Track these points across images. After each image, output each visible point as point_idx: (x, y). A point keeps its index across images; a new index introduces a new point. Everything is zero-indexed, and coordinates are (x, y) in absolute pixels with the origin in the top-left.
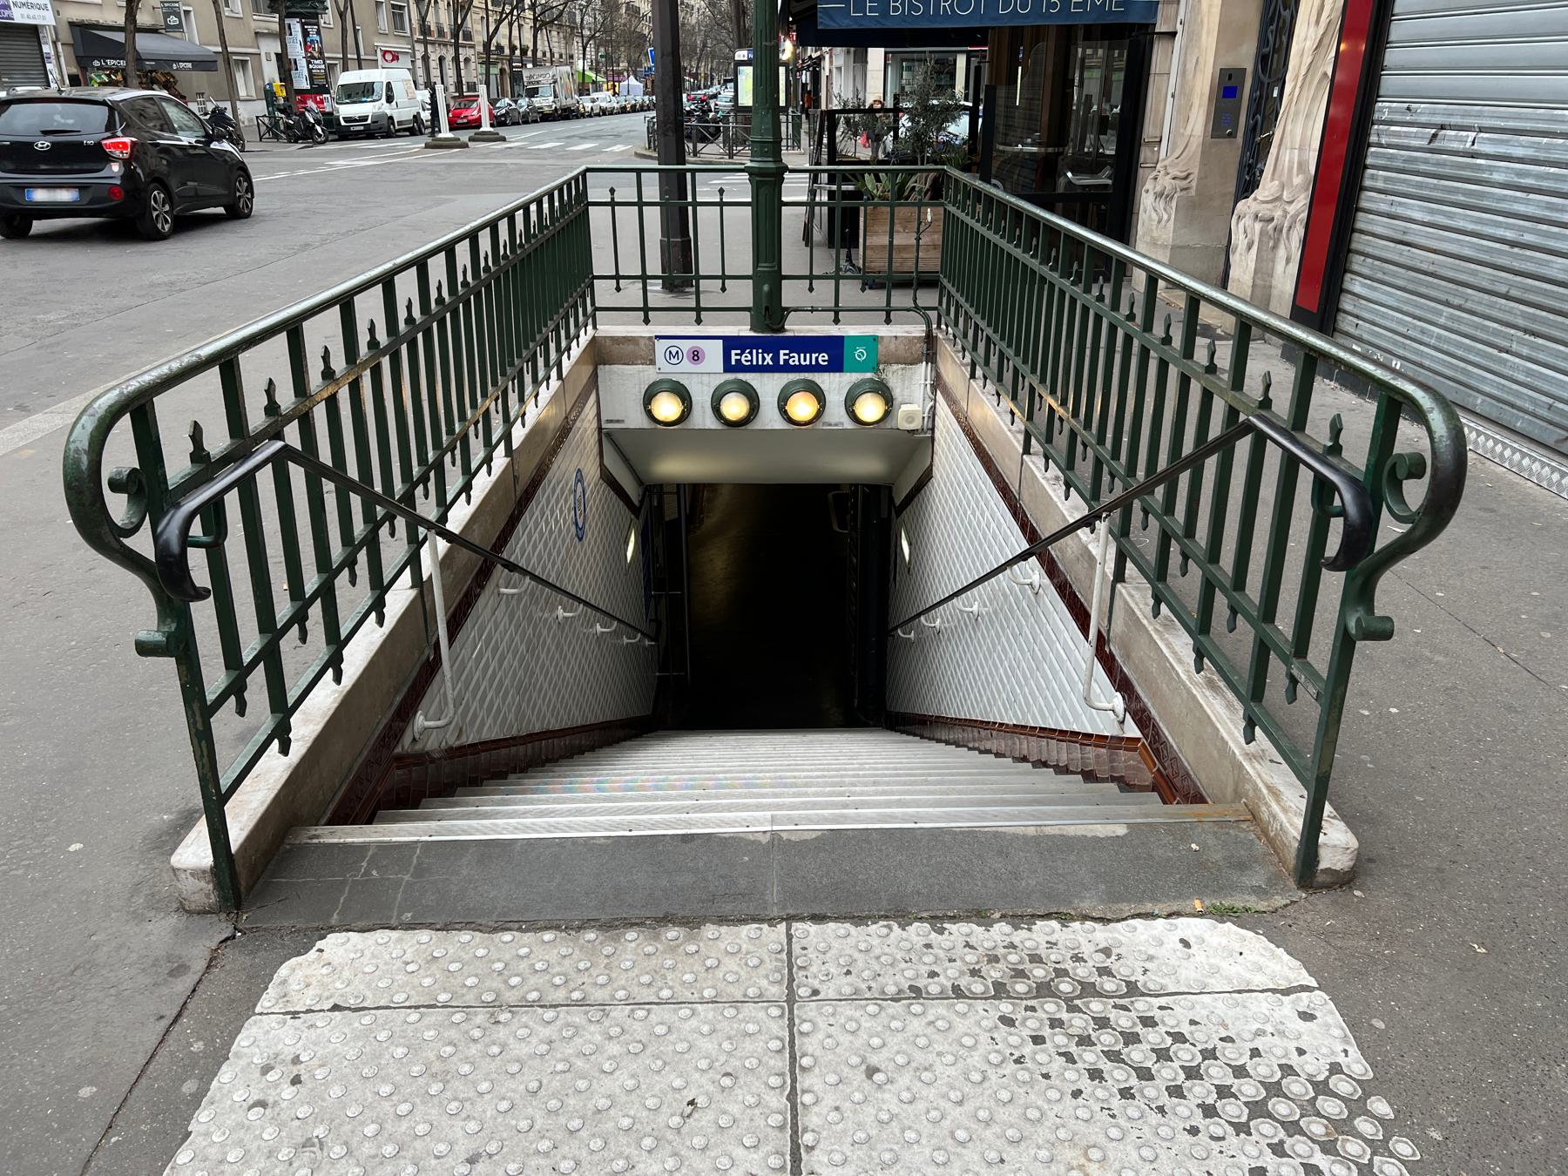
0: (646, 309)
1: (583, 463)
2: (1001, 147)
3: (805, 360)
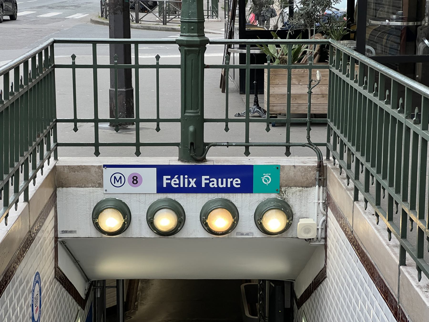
0: (97, 145)
1: (41, 266)
2: (373, 22)
3: (222, 184)
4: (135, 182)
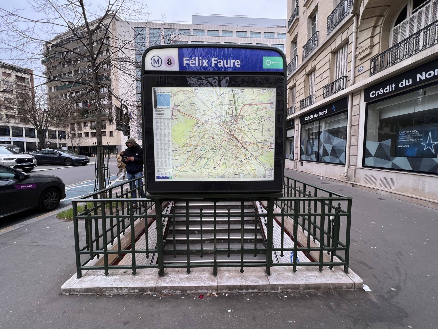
3: (227, 64)
4: (169, 63)
